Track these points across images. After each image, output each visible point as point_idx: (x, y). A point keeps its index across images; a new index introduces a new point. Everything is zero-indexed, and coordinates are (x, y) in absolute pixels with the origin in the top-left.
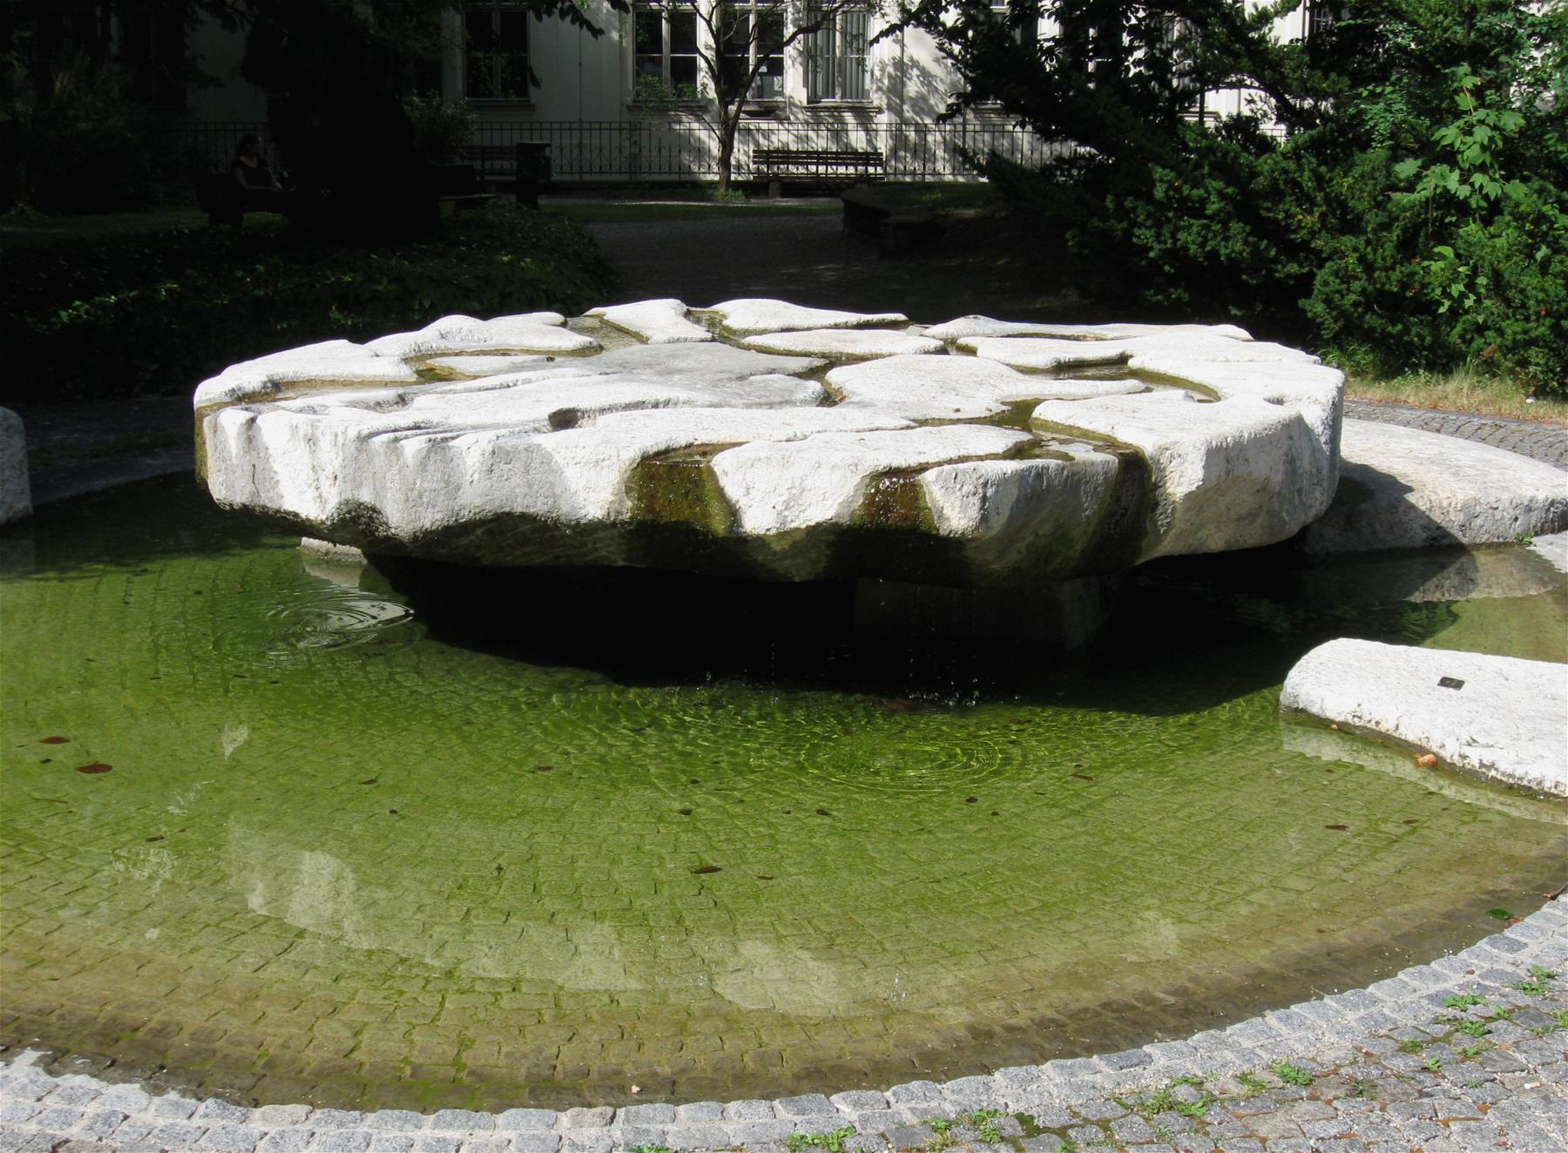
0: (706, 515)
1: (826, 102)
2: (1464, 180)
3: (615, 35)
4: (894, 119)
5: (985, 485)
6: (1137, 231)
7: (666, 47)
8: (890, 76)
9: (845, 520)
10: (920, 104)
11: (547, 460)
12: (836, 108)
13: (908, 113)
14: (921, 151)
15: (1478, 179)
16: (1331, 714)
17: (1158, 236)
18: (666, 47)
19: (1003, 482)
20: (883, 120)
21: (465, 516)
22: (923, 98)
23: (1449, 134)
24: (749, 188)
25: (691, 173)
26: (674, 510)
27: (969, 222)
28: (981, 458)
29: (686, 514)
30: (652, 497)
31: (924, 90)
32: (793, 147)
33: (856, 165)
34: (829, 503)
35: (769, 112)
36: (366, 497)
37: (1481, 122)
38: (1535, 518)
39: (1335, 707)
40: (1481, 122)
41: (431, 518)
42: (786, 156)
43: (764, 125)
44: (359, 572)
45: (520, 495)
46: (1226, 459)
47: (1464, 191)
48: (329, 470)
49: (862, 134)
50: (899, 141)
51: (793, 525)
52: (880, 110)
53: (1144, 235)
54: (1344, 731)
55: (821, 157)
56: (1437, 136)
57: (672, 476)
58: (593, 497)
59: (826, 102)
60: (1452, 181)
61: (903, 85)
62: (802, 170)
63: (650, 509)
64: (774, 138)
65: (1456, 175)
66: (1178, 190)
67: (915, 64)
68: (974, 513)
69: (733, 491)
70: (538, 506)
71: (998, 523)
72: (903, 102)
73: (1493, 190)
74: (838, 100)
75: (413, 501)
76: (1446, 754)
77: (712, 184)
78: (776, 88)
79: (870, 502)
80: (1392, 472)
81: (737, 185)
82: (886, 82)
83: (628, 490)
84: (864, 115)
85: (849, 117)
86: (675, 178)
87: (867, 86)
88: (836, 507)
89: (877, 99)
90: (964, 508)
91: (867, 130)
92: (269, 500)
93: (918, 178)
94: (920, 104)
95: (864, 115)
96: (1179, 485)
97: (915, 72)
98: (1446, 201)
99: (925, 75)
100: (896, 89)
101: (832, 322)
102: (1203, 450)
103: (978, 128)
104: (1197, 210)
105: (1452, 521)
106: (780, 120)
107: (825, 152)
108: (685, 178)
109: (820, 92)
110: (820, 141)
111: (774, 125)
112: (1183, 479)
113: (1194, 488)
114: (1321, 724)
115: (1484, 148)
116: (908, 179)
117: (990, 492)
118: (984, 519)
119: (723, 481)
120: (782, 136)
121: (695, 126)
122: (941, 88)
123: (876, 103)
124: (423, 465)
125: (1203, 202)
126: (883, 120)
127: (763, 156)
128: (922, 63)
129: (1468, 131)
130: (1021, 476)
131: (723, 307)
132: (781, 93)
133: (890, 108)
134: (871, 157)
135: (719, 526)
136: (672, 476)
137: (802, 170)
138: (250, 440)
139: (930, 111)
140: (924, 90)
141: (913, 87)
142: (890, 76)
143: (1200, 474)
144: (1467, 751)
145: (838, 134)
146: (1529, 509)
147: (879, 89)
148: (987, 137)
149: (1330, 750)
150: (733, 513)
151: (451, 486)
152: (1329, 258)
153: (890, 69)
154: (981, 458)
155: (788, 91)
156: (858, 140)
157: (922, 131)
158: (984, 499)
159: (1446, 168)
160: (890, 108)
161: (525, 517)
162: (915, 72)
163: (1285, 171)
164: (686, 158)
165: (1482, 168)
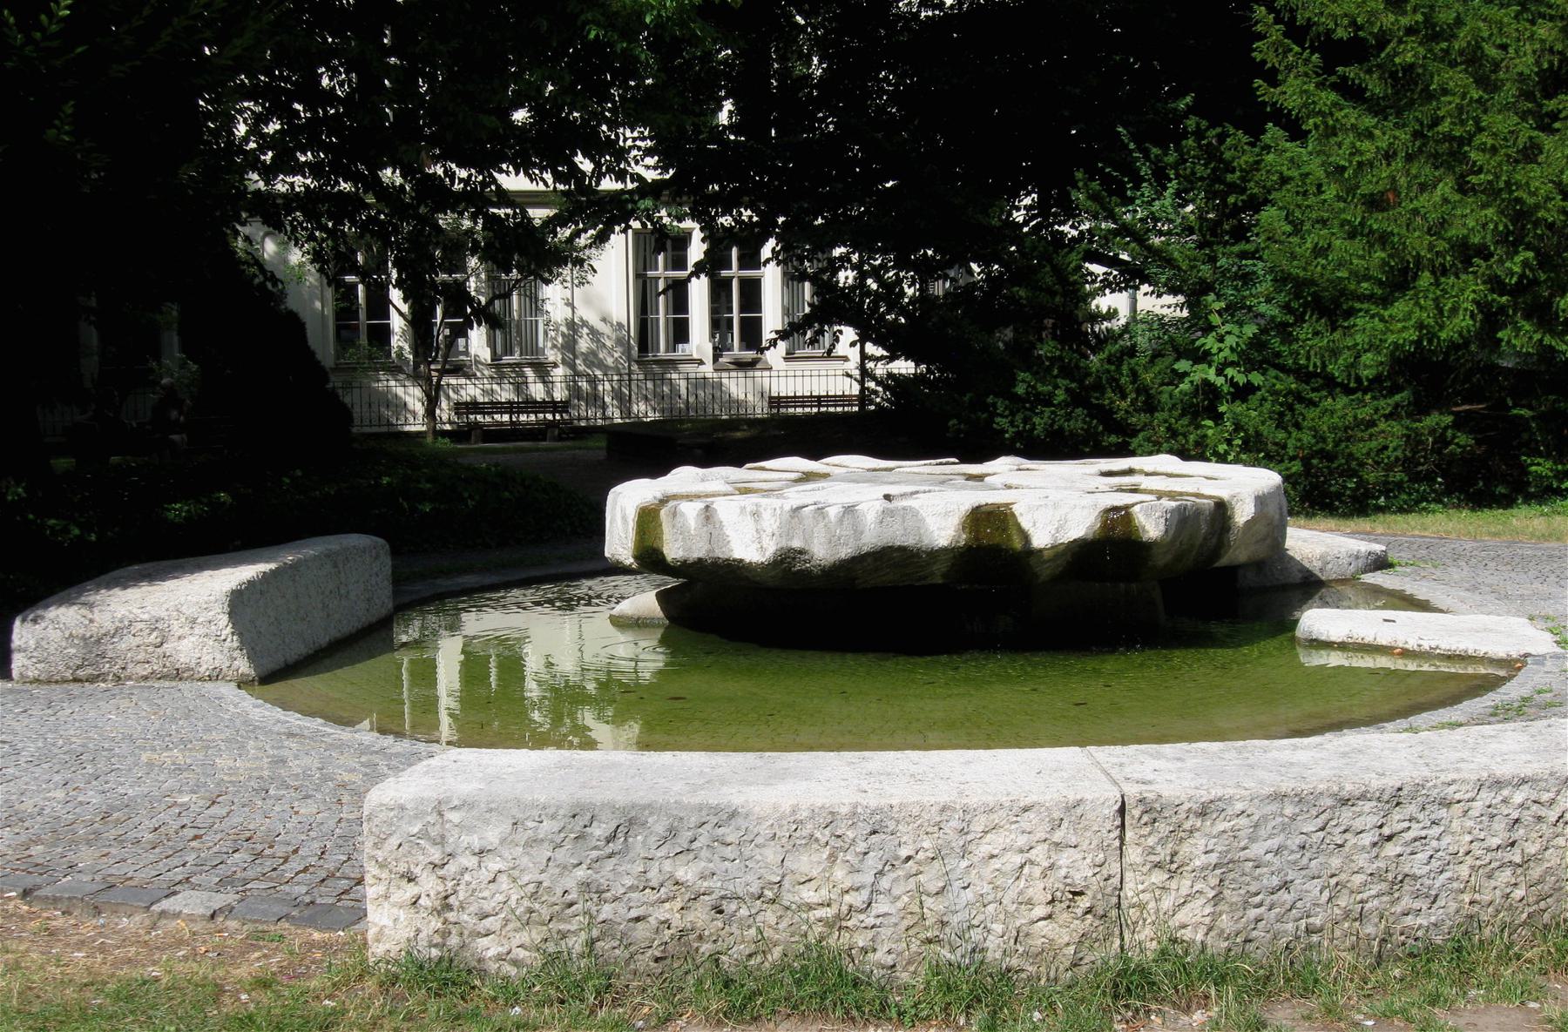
0: (1009, 537)
1: (507, 359)
2: (1220, 372)
3: (318, 305)
4: (569, 372)
6: (998, 419)
7: (362, 314)
8: (563, 335)
9: (1090, 536)
10: (592, 359)
11: (915, 513)
12: (518, 365)
13: (581, 368)
14: (595, 399)
15: (1230, 372)
16: (1333, 639)
17: (1012, 423)
18: (362, 314)
19: (1173, 511)
20: (559, 372)
21: (865, 549)
22: (594, 353)
23: (1210, 342)
24: (459, 435)
25: (389, 424)
26: (989, 536)
27: (739, 440)
29: (997, 540)
30: (977, 532)
31: (594, 346)
32: (480, 399)
33: (536, 413)
35: (458, 370)
36: (797, 544)
37: (1229, 333)
38: (1361, 563)
40: (1229, 333)
41: (845, 552)
42: (474, 406)
43: (453, 381)
44: (659, 633)
45: (898, 535)
47: (1220, 381)
48: (769, 531)
49: (540, 386)
50: (575, 391)
52: (555, 365)
53: (1001, 422)
54: (1342, 646)
55: (509, 407)
56: (1198, 343)
57: (990, 523)
58: (943, 533)
59: (507, 359)
60: (1211, 375)
61: (575, 342)
62: (488, 419)
63: (977, 539)
64: (463, 393)
65: (1212, 371)
66: (1034, 387)
67: (585, 323)
68: (1162, 527)
69: (1025, 523)
70: (909, 541)
71: (1171, 533)
72: (575, 357)
73: (1241, 379)
74: (516, 357)
75: (832, 541)
76: (1409, 647)
77: (419, 433)
78: (461, 349)
79: (1104, 526)
81: (444, 433)
82: (560, 340)
83: (964, 528)
84: (542, 370)
85: (529, 372)
86: (384, 429)
87: (541, 345)
89: (552, 355)
90: (1157, 525)
91: (544, 382)
92: (721, 554)
93: (592, 423)
94: (592, 359)
95: (542, 370)
97: (585, 330)
98: (1207, 387)
99: (594, 332)
100: (570, 345)
103: (641, 377)
104: (1047, 401)
105: (1315, 566)
106: (468, 377)
107: (509, 402)
108: (392, 429)
109: (499, 350)
110: (505, 394)
111: (462, 381)
114: (1328, 645)
115: (1231, 348)
116: (583, 424)
119: (1020, 520)
120: (471, 391)
121: (392, 383)
122: (608, 343)
123: (551, 359)
124: (841, 521)
125: (1051, 395)
126: (559, 372)
127: (463, 408)
128: (591, 322)
129: (1221, 339)
130: (1178, 507)
132: (466, 353)
133: (564, 362)
134: (553, 406)
135: (1017, 544)
136: (990, 523)
137: (488, 419)
138: (707, 518)
139: (601, 365)
140: (594, 346)
141: (584, 344)
142: (563, 335)
145: (520, 387)
146: (1357, 557)
147: (554, 346)
148: (650, 385)
149: (1335, 659)
150: (1026, 537)
151: (858, 532)
152: (1142, 430)
153: (564, 329)
155: (472, 351)
156: (537, 391)
157: (593, 381)
159: (1205, 366)
160: (564, 362)
161: (902, 549)
162: (585, 330)
163: (1108, 371)
164: (386, 412)
165: (1232, 364)
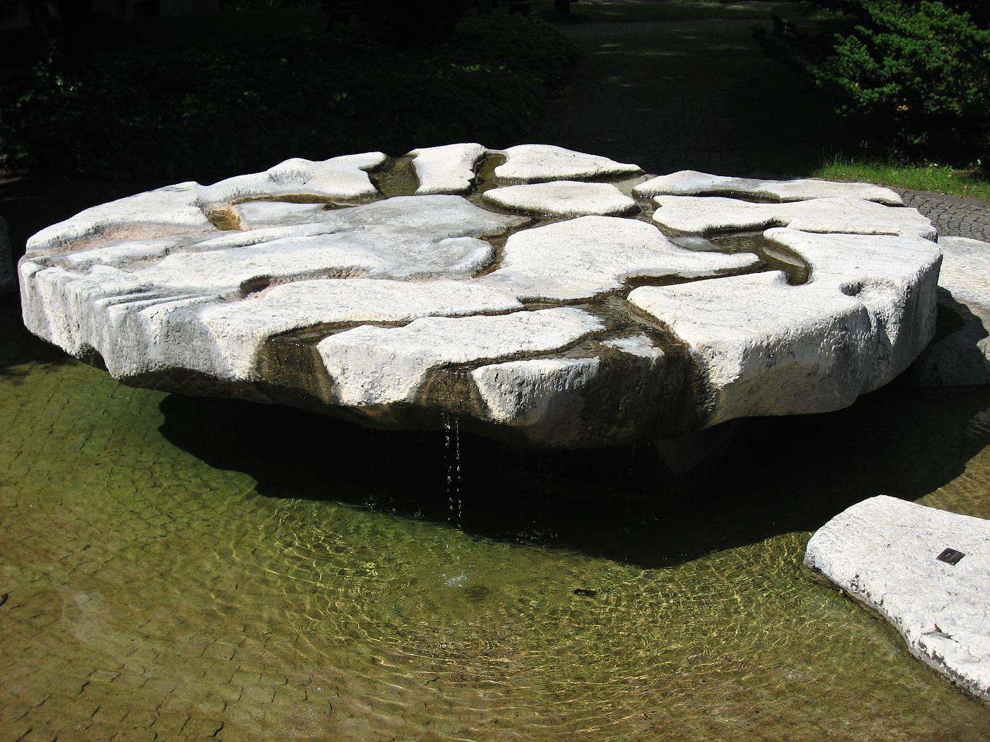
5: (521, 384)
28: (498, 361)
34: (402, 387)
39: (841, 573)
46: (763, 358)
51: (377, 401)
68: (511, 407)
80: (670, 583)
88: (407, 390)
90: (503, 404)
96: (721, 377)
101: (592, 170)
102: (741, 350)
112: (724, 372)
113: (732, 380)
117: (526, 390)
118: (520, 413)
131: (27, 245)
136: (293, 349)
143: (738, 369)
144: (927, 641)
151: (142, 346)
154: (498, 361)
158: (520, 396)
